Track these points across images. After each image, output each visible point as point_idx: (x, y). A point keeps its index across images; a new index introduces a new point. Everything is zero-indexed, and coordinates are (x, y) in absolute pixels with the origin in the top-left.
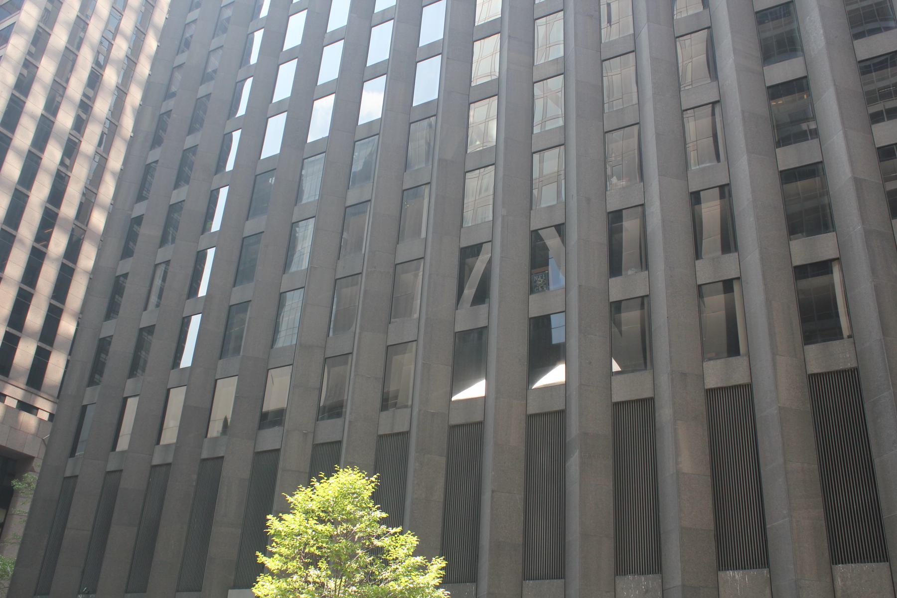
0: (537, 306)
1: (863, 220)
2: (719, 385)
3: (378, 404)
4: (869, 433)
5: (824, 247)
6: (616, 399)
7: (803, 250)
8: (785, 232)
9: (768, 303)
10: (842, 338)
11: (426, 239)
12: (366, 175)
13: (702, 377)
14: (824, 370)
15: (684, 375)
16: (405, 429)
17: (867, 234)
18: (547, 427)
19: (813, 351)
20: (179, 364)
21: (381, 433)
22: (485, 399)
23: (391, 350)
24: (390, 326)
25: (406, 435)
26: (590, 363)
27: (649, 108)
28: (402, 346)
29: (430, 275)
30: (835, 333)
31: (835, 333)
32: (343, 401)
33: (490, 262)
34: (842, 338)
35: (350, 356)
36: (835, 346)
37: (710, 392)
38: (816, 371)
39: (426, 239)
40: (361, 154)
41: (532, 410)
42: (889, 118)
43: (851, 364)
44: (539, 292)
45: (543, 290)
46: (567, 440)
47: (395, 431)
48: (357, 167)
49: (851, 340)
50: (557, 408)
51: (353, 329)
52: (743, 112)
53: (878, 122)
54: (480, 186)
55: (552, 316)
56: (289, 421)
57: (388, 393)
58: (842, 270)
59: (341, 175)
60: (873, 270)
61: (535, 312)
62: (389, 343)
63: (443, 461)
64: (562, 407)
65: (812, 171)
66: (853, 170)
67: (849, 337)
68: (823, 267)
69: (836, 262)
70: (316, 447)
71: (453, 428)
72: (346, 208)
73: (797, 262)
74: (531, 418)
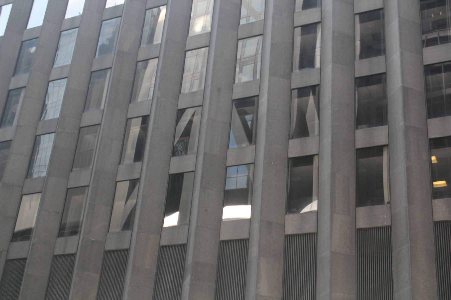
0: (177, 165)
1: (405, 118)
2: (295, 233)
3: (56, 232)
4: (393, 273)
5: (308, 146)
6: (223, 238)
7: (365, 137)
8: (353, 123)
9: (333, 175)
10: (384, 204)
11: (104, 110)
12: (105, 50)
13: (283, 226)
14: (368, 226)
15: (270, 223)
16: (73, 251)
17: (407, 129)
18: (233, 251)
19: (362, 211)
20: (32, 174)
21: (56, 253)
22: (250, 221)
23: (70, 192)
24: (71, 173)
25: (73, 255)
26: (206, 211)
27: (270, 22)
28: (82, 189)
29: (102, 137)
30: (379, 199)
31: (379, 199)
32: (79, 222)
33: (190, 122)
34: (384, 204)
35: (87, 188)
36: (378, 209)
37: (288, 237)
38: (363, 226)
39: (104, 110)
40: (108, 30)
41: (163, 243)
42: (442, 43)
43: (387, 223)
44: (179, 155)
45: (182, 154)
46: (185, 267)
47: (67, 253)
48: (103, 40)
49: (389, 205)
50: (181, 242)
51: (91, 167)
52: (333, 32)
53: (427, 46)
54: (57, 94)
55: (185, 174)
56: (34, 238)
57: (65, 224)
58: (389, 154)
59: (89, 46)
60: (407, 156)
61: (174, 170)
62: (69, 187)
63: (98, 276)
64: (184, 242)
65: (379, 79)
66: (403, 81)
67: (388, 203)
68: (378, 150)
69: (386, 147)
70: (8, 261)
71: (108, 252)
72: (92, 72)
73: (359, 146)
74: (162, 248)
